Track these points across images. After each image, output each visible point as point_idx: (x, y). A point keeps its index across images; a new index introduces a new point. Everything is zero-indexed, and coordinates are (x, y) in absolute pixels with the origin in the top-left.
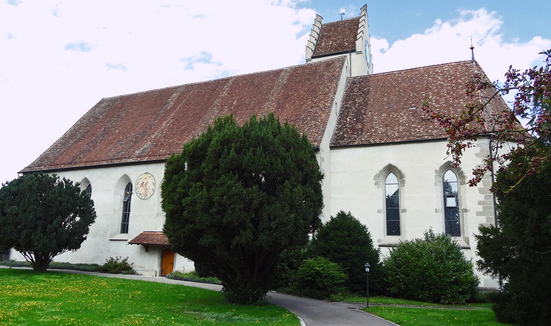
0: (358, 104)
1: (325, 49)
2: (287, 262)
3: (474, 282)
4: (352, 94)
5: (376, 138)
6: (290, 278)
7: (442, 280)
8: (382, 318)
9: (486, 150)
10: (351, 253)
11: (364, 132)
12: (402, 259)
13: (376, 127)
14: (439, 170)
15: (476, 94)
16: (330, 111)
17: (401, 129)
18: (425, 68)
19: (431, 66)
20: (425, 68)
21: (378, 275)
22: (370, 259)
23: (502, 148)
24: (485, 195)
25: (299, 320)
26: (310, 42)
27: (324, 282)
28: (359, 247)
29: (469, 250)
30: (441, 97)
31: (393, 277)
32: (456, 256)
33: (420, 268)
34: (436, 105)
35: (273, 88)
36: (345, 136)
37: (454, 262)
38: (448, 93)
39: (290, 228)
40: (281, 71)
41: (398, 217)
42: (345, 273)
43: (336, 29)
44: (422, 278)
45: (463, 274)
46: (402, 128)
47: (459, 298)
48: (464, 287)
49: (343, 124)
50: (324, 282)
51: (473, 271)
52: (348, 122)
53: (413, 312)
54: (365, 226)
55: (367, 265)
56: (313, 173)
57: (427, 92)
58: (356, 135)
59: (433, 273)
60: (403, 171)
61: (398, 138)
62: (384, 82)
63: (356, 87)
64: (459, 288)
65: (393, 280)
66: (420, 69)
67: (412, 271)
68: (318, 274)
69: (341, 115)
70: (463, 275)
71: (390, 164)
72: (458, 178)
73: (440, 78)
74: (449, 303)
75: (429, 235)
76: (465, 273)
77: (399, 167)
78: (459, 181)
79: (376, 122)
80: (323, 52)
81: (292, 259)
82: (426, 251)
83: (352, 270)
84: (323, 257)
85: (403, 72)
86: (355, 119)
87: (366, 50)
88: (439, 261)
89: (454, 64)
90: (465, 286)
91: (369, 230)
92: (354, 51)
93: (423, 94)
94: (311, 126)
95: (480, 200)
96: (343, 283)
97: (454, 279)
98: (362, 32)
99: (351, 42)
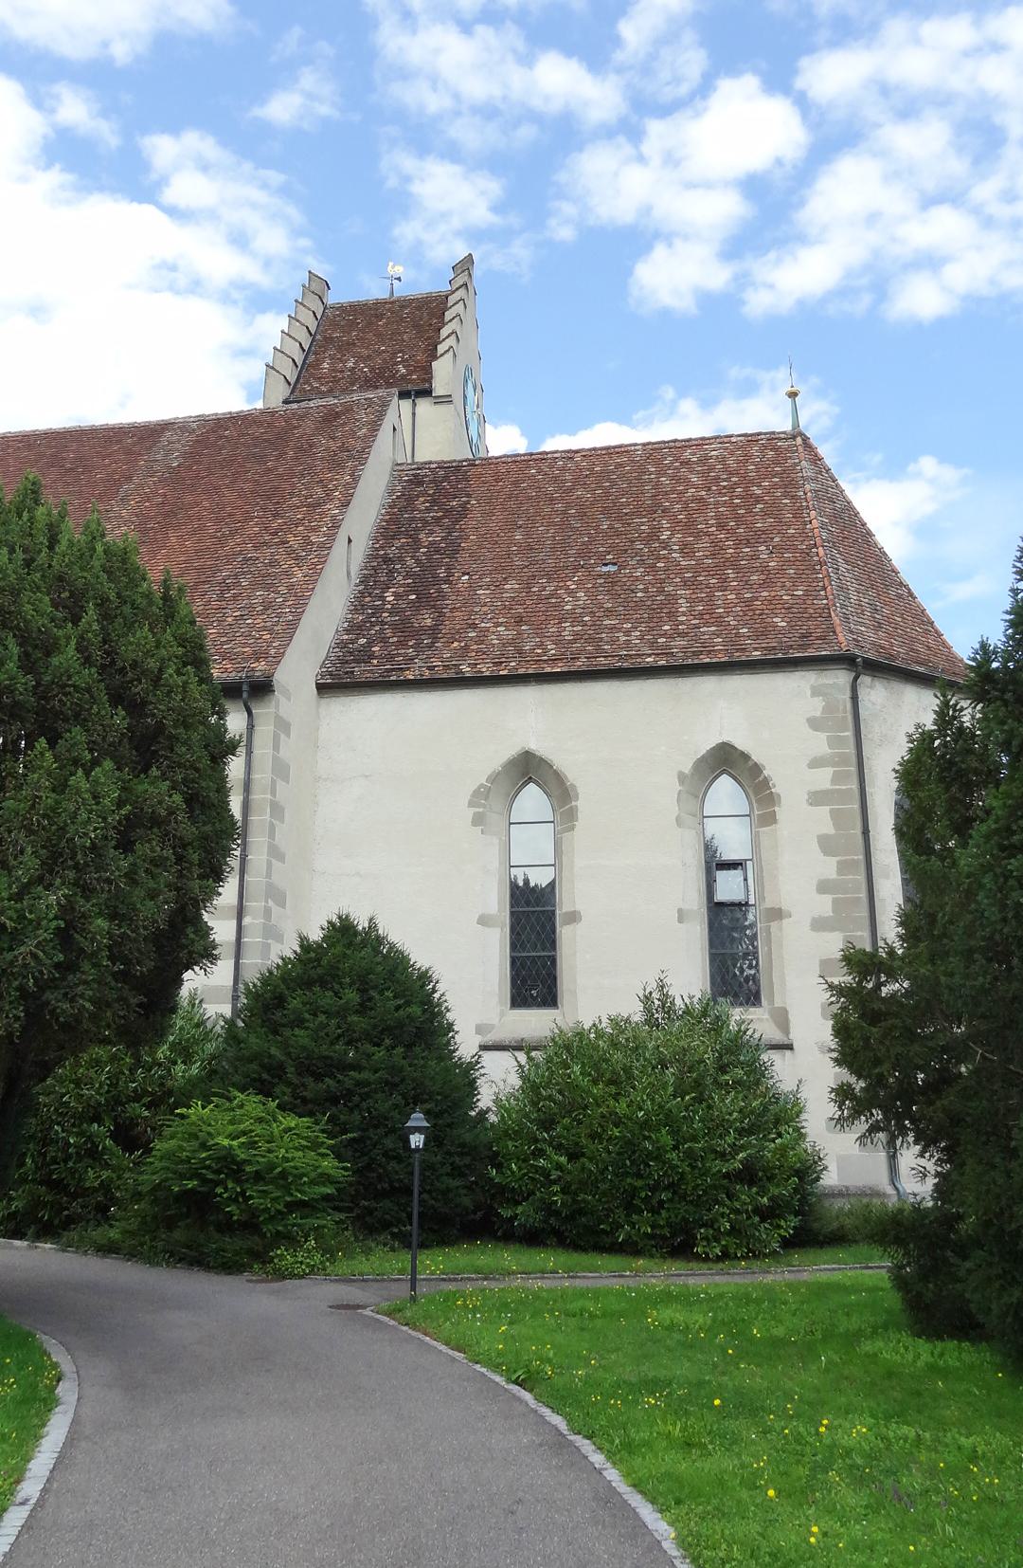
0: (425, 547)
1: (332, 382)
2: (115, 1119)
3: (807, 1171)
4: (406, 516)
5: (483, 659)
6: (118, 1188)
7: (700, 1169)
8: (456, 1355)
9: (841, 708)
10: (365, 1075)
11: (442, 640)
12: (560, 1092)
13: (483, 625)
14: (692, 774)
15: (806, 531)
16: (324, 559)
17: (567, 633)
18: (650, 447)
19: (668, 442)
20: (650, 447)
21: (467, 1160)
22: (439, 1098)
23: (815, 846)
24: (838, 858)
25: (37, 1403)
26: (282, 352)
27: (251, 1197)
28: (400, 1050)
29: (788, 1053)
30: (698, 535)
31: (523, 1165)
32: (748, 1077)
33: (624, 1123)
34: (681, 559)
35: (129, 479)
36: (374, 651)
37: (741, 1096)
38: (721, 526)
39: (34, 956)
40: (163, 427)
41: (549, 940)
42: (339, 1157)
43: (370, 324)
44: (628, 1162)
45: (773, 1140)
46: (571, 628)
47: (759, 1231)
48: (776, 1192)
49: (370, 611)
50: (251, 1197)
51: (803, 1127)
52: (389, 606)
53: (590, 1313)
54: (427, 971)
55: (418, 1119)
56: (187, 726)
57: (654, 520)
58: (412, 647)
59: (669, 1141)
60: (572, 774)
61: (555, 660)
62: (516, 483)
63: (424, 494)
64: (757, 1193)
65: (525, 1175)
66: (633, 448)
67: (594, 1136)
68: (226, 1167)
69: (364, 580)
70: (773, 1145)
71: (527, 752)
72: (754, 801)
73: (696, 479)
74: (725, 1256)
75: (657, 1002)
76: (780, 1135)
77: (560, 761)
78: (756, 813)
79: (485, 609)
80: (323, 388)
81: (137, 1105)
82: (645, 1060)
83: (368, 1142)
84: (257, 1094)
85: (579, 455)
86: (414, 597)
87: (465, 397)
88: (689, 1094)
89: (739, 438)
90: (778, 1186)
91: (441, 988)
92: (426, 393)
93: (643, 524)
94: (252, 607)
95: (822, 878)
96: (327, 1198)
97: (741, 1162)
98: (453, 337)
99: (418, 367)
